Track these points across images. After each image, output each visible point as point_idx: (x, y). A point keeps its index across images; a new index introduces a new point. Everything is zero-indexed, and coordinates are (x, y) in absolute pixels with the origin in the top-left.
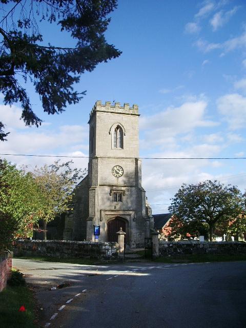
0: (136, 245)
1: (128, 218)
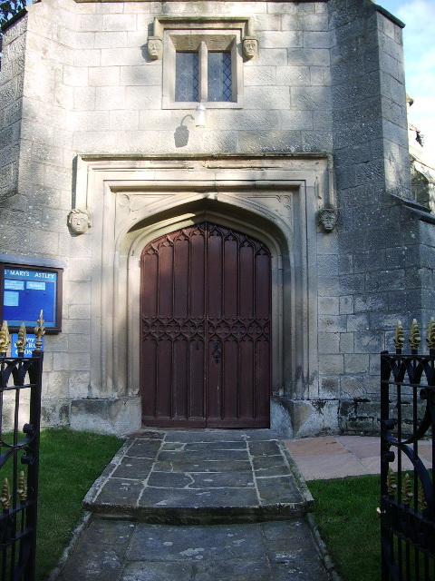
0: (344, 407)
1: (276, 207)
